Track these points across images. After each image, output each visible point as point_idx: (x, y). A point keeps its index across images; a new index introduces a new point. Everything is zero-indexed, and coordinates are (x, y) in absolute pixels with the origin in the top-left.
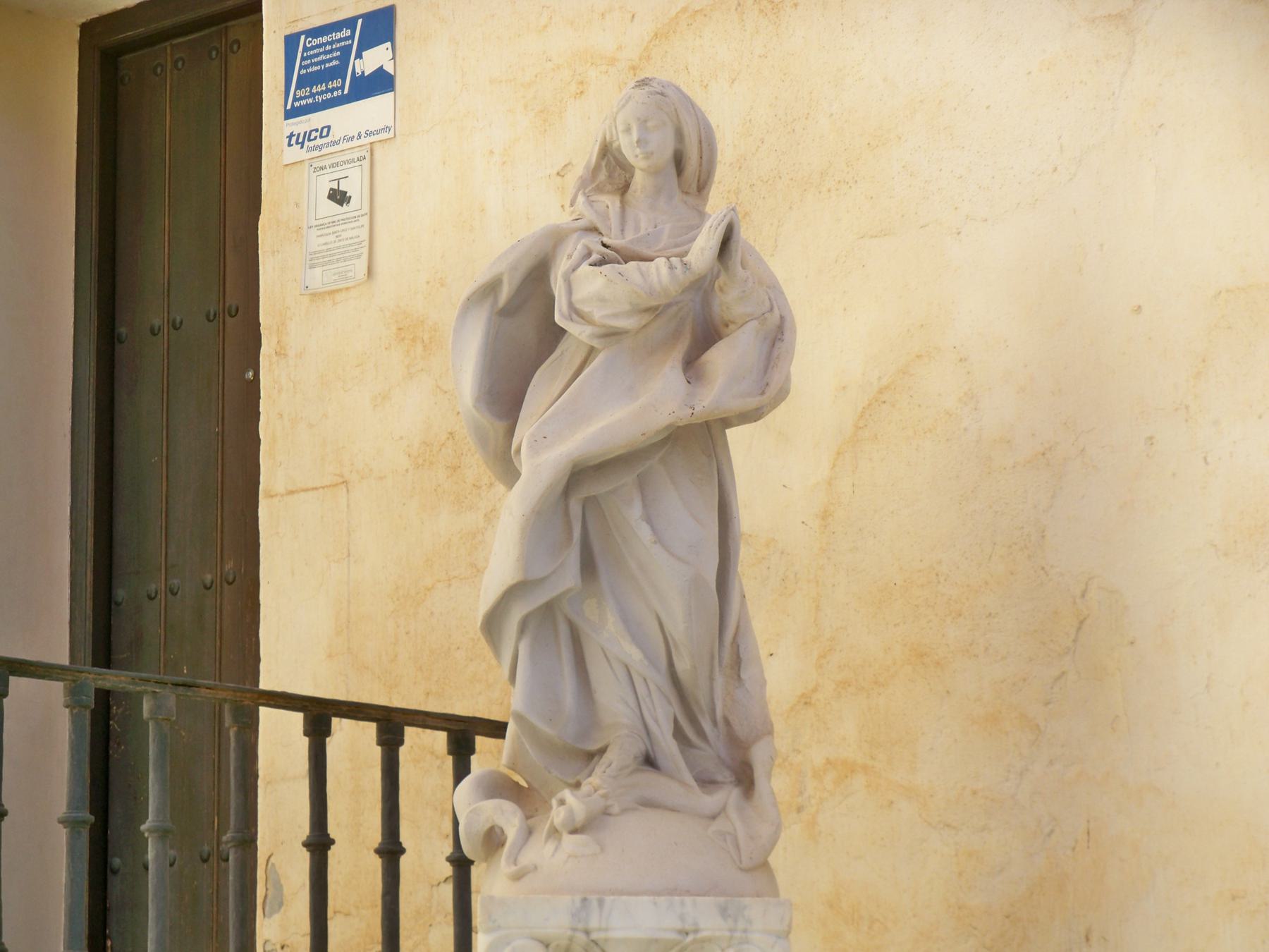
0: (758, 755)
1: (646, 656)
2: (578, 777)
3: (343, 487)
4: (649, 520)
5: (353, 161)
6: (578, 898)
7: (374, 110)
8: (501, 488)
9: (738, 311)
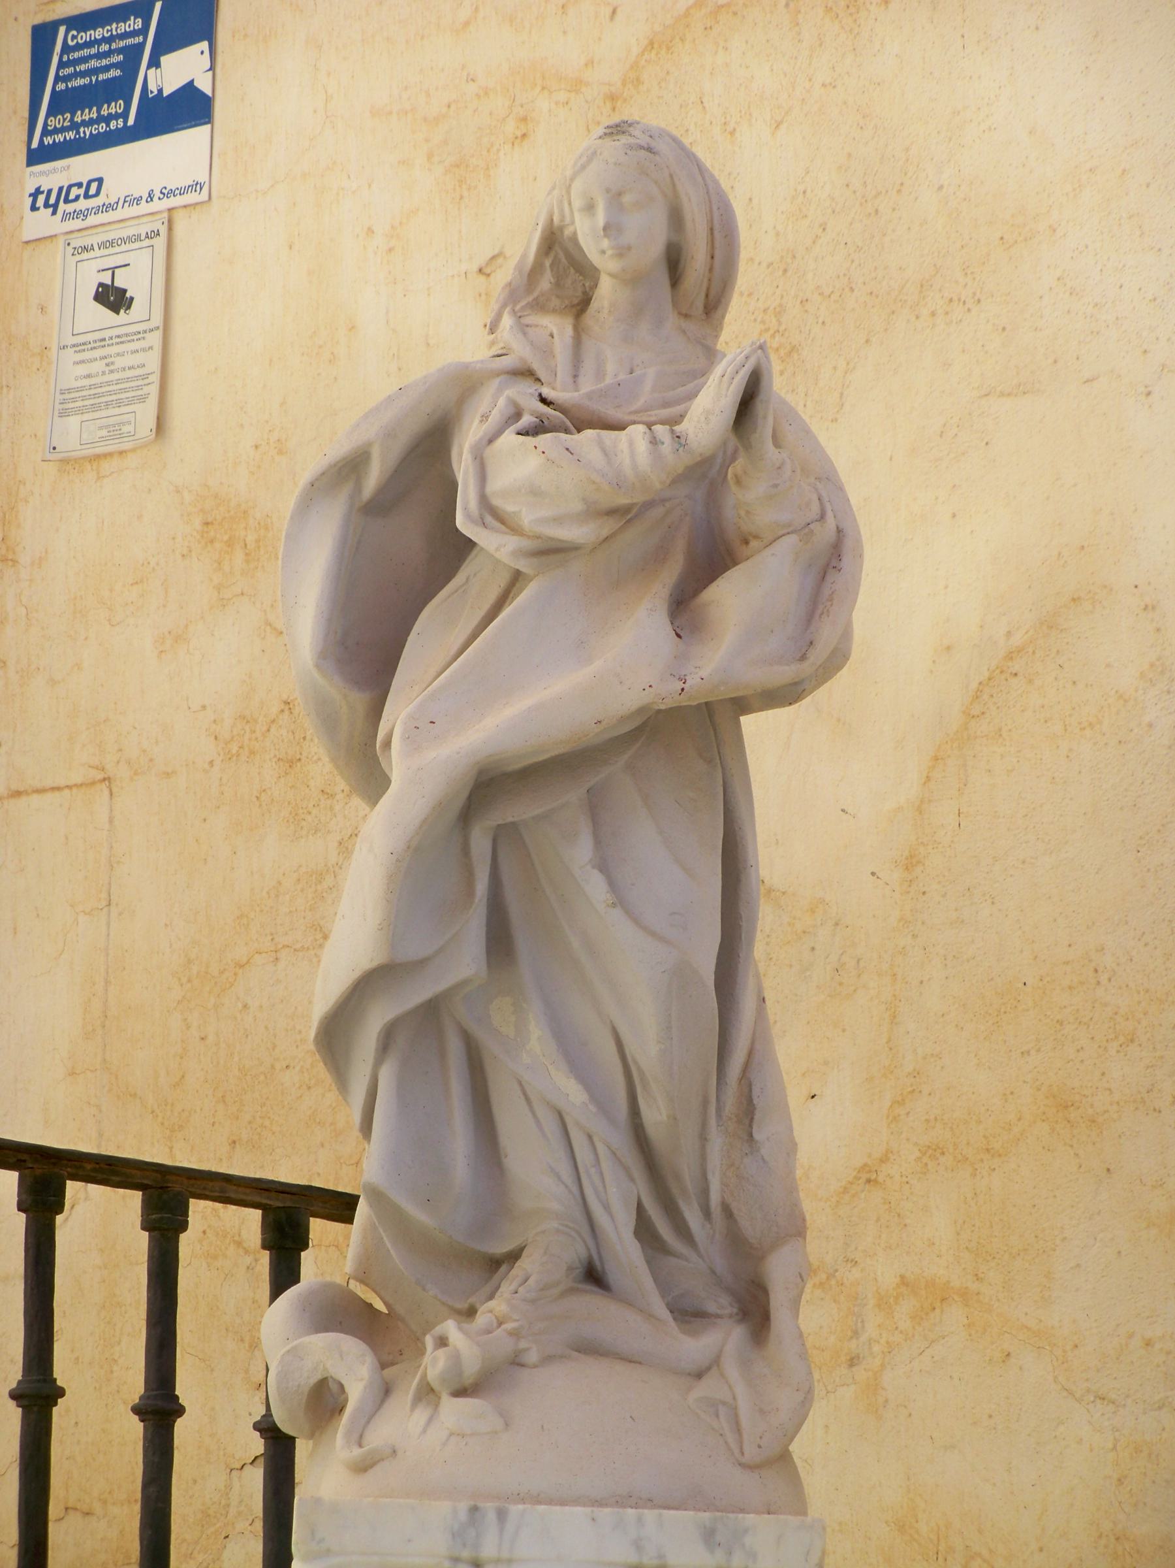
0: (778, 1271)
1: (593, 1098)
2: (472, 1300)
3: (104, 786)
4: (603, 866)
5: (138, 238)
6: (463, 1507)
7: (174, 155)
8: (357, 802)
9: (764, 517)
